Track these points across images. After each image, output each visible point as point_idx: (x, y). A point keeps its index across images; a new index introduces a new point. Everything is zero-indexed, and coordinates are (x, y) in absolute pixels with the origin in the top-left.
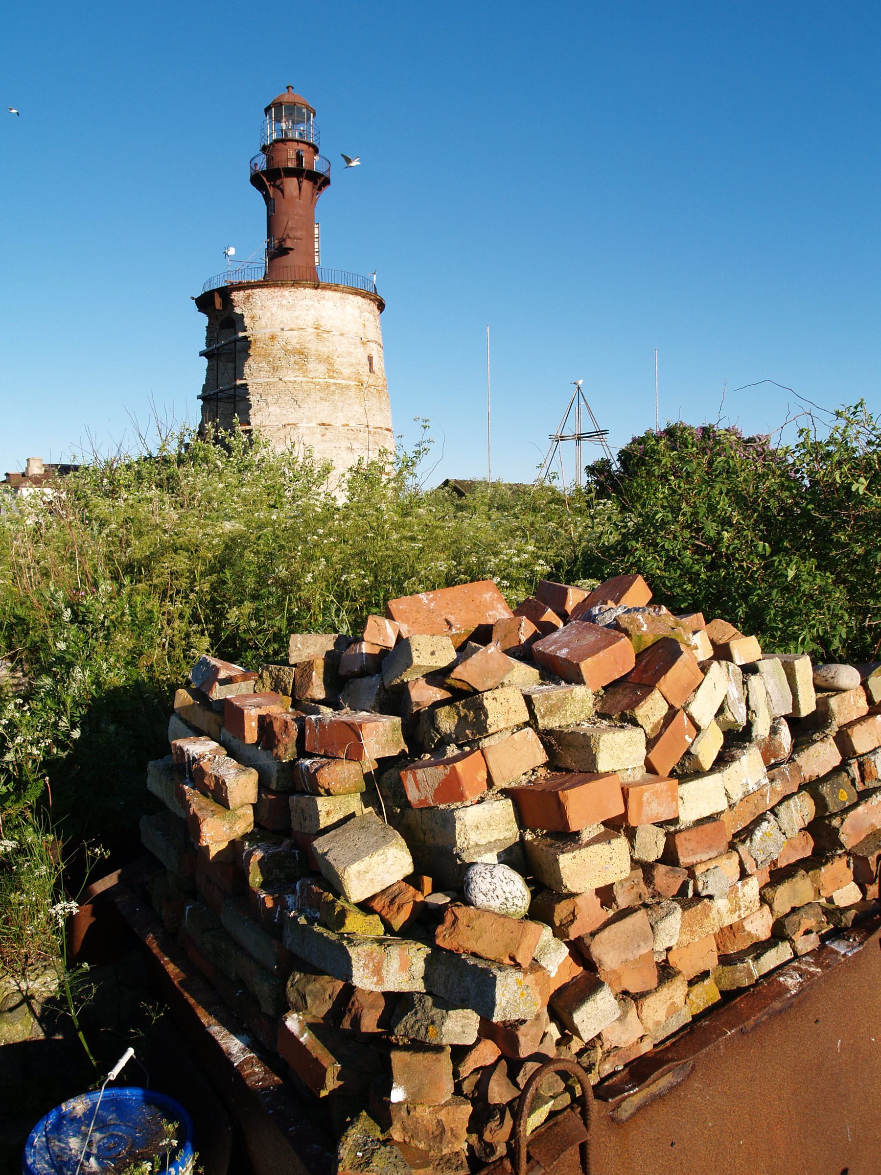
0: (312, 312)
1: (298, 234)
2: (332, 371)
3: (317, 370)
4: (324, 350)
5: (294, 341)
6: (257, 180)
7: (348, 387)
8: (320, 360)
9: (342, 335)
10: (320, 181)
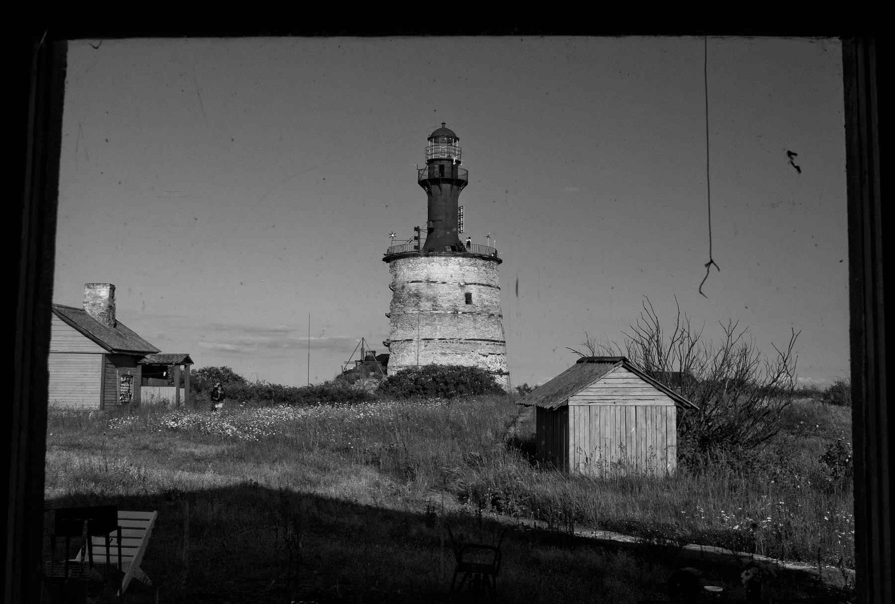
0: (425, 270)
1: (440, 218)
2: (435, 306)
3: (426, 305)
4: (430, 292)
5: (414, 289)
6: (422, 183)
7: (445, 315)
8: (428, 299)
9: (444, 283)
10: (462, 183)
